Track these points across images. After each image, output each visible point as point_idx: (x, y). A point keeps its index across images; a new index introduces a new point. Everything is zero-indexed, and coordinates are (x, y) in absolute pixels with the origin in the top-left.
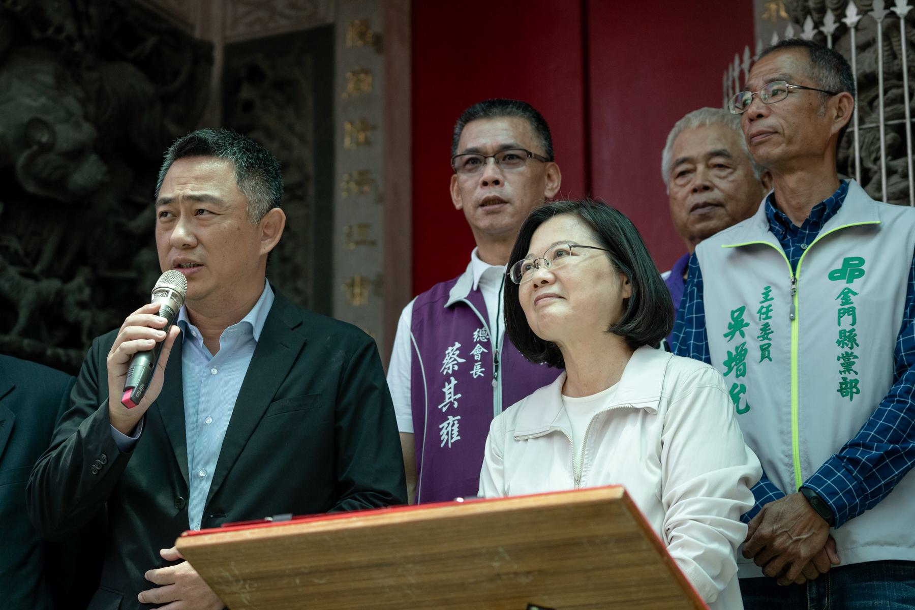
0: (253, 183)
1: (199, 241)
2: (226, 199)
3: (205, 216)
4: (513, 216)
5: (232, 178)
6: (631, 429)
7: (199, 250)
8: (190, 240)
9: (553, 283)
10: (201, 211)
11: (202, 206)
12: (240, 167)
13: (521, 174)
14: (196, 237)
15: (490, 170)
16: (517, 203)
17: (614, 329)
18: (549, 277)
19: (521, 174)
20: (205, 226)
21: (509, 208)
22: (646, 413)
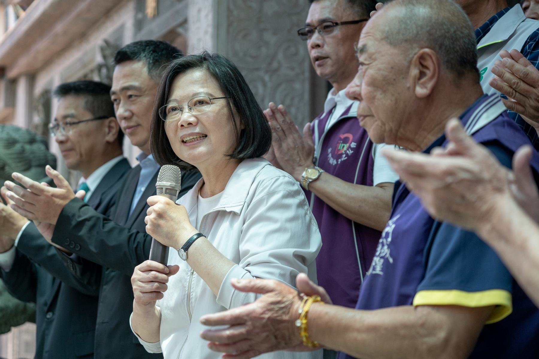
0: (158, 72)
1: (133, 114)
2: (143, 86)
3: (133, 98)
4: (332, 66)
5: (145, 70)
6: (225, 224)
7: (135, 119)
8: (127, 114)
9: (197, 124)
10: (130, 96)
11: (130, 93)
12: (149, 63)
13: (334, 37)
14: (131, 111)
15: (315, 38)
16: (334, 57)
17: (232, 156)
18: (192, 120)
19: (334, 37)
20: (134, 104)
21: (329, 62)
22: (235, 215)
